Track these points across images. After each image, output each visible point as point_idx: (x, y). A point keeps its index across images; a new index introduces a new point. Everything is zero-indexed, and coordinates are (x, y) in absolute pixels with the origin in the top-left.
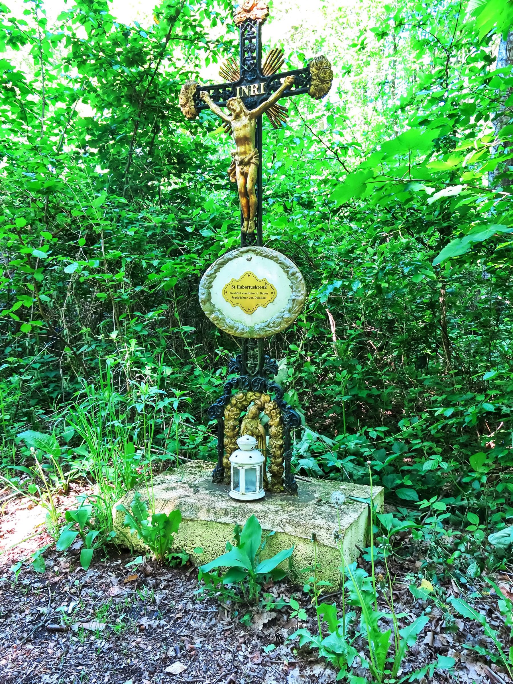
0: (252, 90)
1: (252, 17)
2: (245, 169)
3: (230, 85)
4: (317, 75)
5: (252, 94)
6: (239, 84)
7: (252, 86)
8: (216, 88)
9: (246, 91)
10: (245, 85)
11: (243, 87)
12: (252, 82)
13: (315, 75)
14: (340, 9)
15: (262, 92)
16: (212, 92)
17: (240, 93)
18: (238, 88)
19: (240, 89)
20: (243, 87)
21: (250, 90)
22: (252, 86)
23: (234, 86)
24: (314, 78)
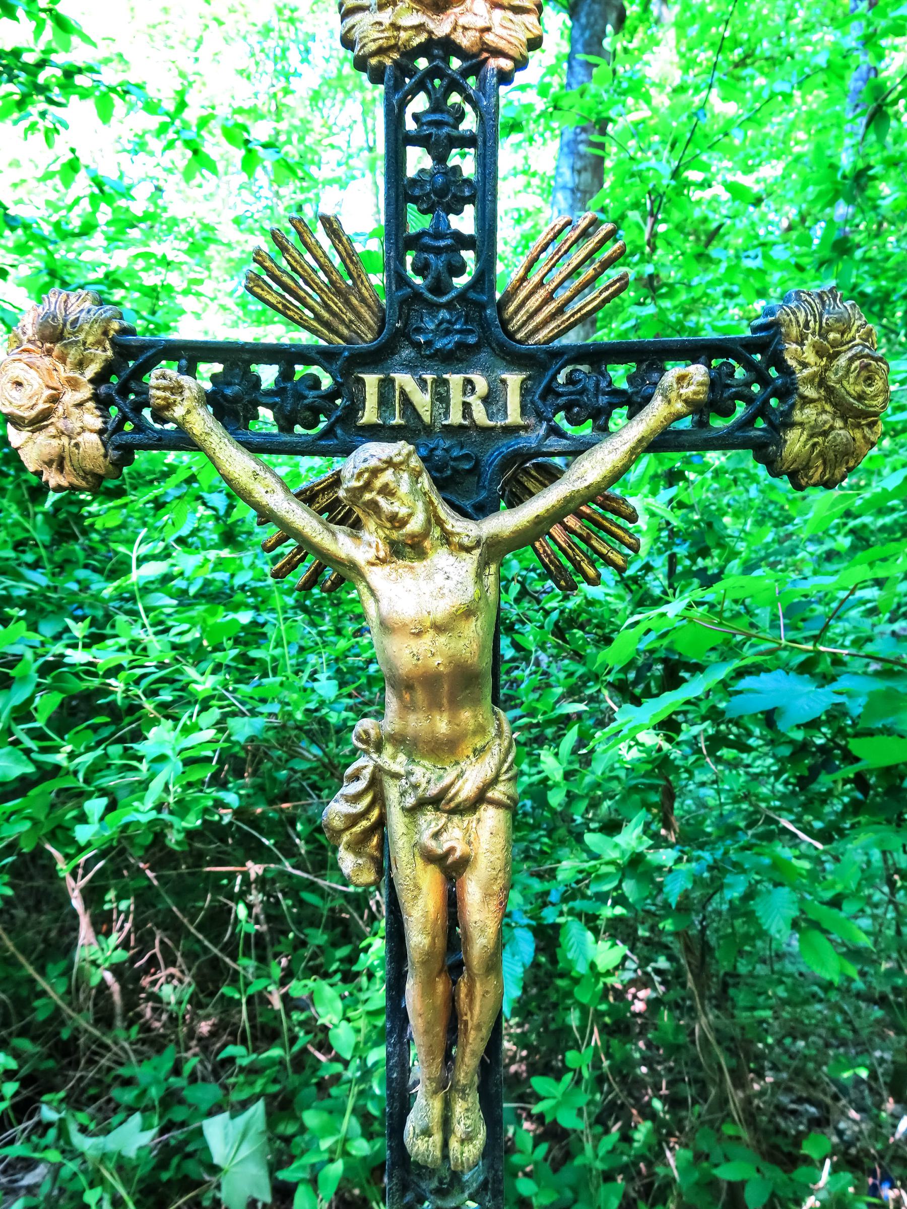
0: (456, 398)
1: (465, 41)
2: (453, 838)
3: (325, 357)
4: (821, 381)
5: (456, 417)
6: (375, 358)
7: (455, 380)
8: (237, 357)
9: (422, 400)
10: (410, 367)
11: (404, 380)
12: (455, 358)
13: (810, 380)
14: (165, 10)
15: (514, 416)
16: (208, 370)
17: (384, 401)
18: (371, 380)
19: (386, 385)
20: (404, 380)
21: (442, 399)
22: (455, 380)
23: (349, 363)
24: (810, 392)
